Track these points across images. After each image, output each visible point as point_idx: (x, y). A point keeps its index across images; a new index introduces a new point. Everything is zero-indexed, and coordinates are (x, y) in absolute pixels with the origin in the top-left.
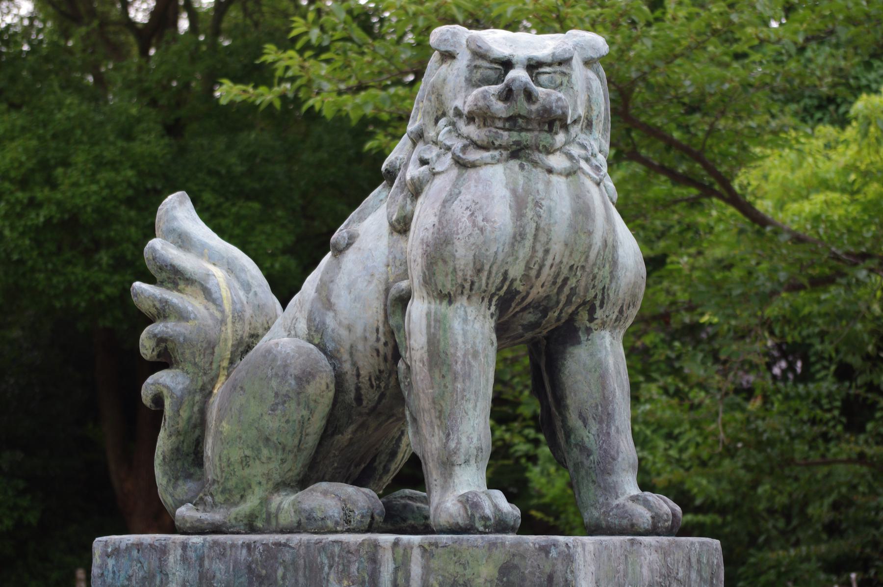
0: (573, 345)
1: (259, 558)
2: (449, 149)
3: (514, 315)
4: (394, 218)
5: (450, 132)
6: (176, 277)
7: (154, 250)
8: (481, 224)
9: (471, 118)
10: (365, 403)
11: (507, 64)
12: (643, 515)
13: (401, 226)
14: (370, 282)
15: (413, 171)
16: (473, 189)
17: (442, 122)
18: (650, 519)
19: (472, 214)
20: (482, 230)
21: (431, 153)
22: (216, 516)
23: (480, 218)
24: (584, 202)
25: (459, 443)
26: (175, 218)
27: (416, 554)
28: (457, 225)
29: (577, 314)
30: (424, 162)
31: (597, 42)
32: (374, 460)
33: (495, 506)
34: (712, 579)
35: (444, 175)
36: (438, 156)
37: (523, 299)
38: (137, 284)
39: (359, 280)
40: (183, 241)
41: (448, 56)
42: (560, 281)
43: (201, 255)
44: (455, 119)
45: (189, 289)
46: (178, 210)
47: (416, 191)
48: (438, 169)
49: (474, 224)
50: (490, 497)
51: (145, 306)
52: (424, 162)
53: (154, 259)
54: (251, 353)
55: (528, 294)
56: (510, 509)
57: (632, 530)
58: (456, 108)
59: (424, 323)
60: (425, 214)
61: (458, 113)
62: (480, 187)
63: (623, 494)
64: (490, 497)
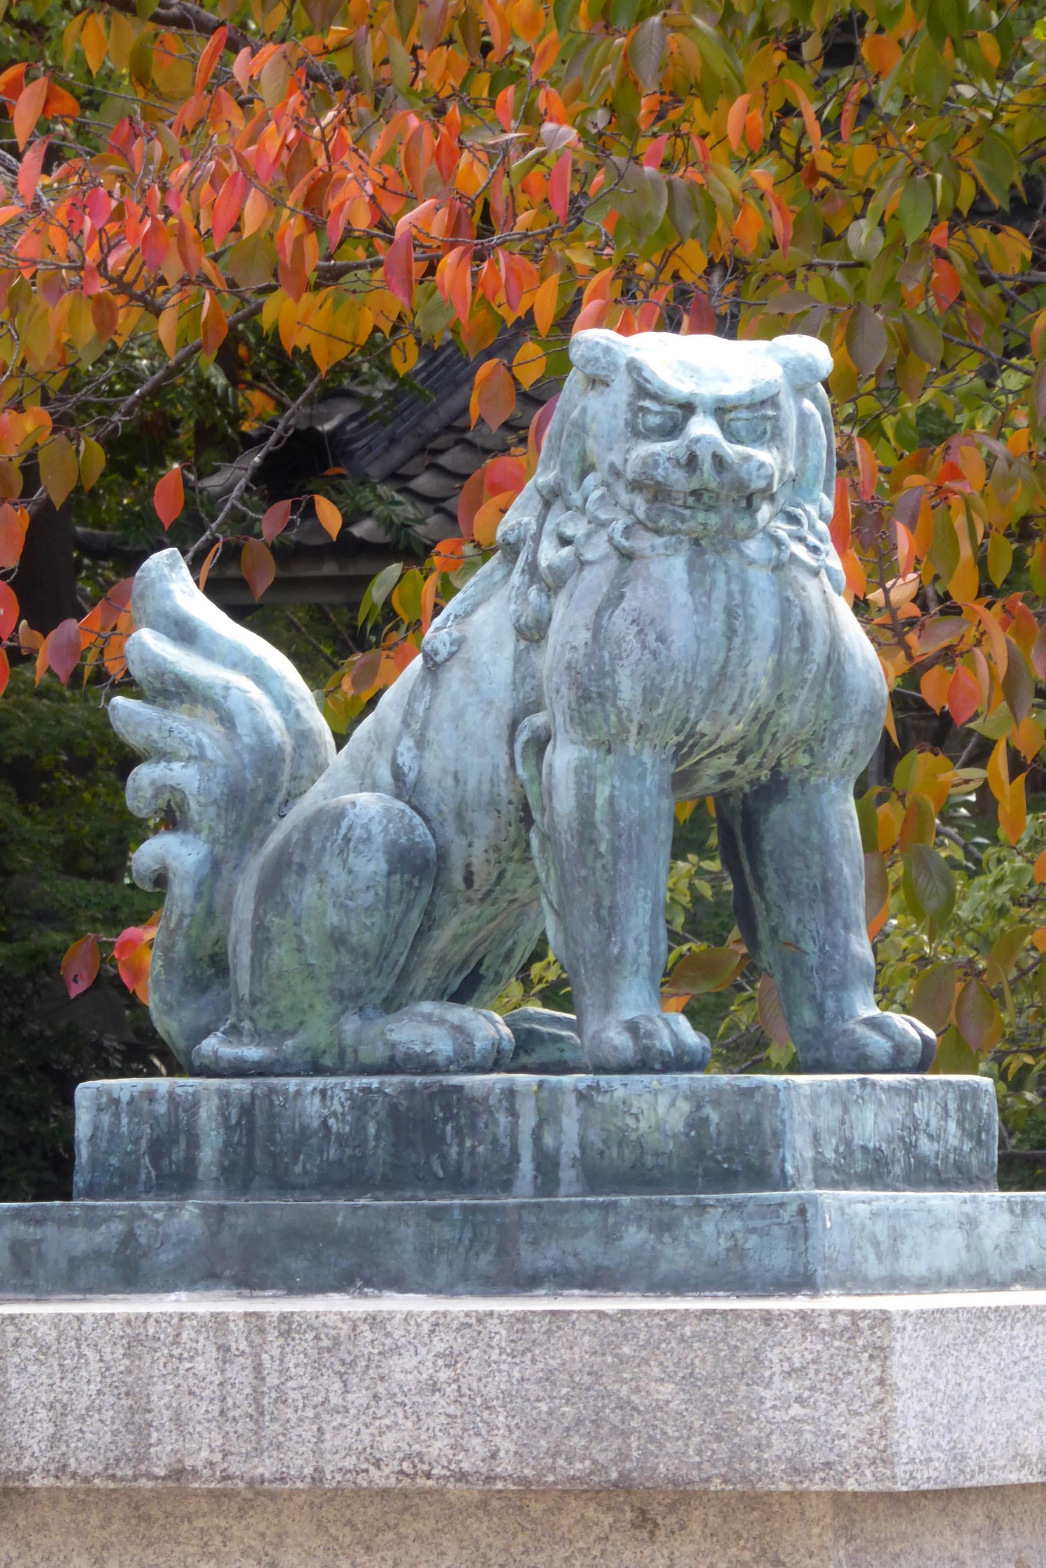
0: (780, 802)
1: (340, 1110)
2: (603, 525)
3: (697, 763)
4: (522, 620)
5: (602, 497)
6: (172, 691)
7: (142, 645)
8: (654, 645)
9: (635, 486)
10: (476, 886)
11: (688, 408)
12: (879, 1045)
13: (532, 633)
14: (487, 713)
15: (549, 554)
16: (641, 592)
17: (590, 480)
18: (99, 607)
19: (640, 632)
20: (655, 654)
21: (576, 529)
22: (252, 1053)
23: (652, 637)
24: (853, 1048)
25: (623, 948)
26: (169, 593)
27: (571, 1099)
28: (619, 646)
29: (965, 1502)
30: (565, 541)
31: (815, 352)
32: (480, 963)
33: (674, 1034)
34: (979, 1133)
35: (596, 567)
36: (589, 536)
37: (711, 743)
38: (119, 700)
39: (471, 709)
40: (184, 632)
41: (597, 382)
42: (762, 717)
43: (209, 655)
44: (610, 480)
45: (200, 709)
46: (171, 579)
47: (552, 583)
48: (589, 555)
49: (644, 647)
50: (667, 1023)
51: (134, 739)
52: (565, 541)
53: (143, 661)
54: (476, 878)
55: (718, 736)
56: (697, 1040)
57: (862, 1063)
58: (612, 465)
59: (572, 779)
60: (569, 621)
61: (616, 473)
62: (652, 590)
63: (852, 1017)
64: (667, 1023)
